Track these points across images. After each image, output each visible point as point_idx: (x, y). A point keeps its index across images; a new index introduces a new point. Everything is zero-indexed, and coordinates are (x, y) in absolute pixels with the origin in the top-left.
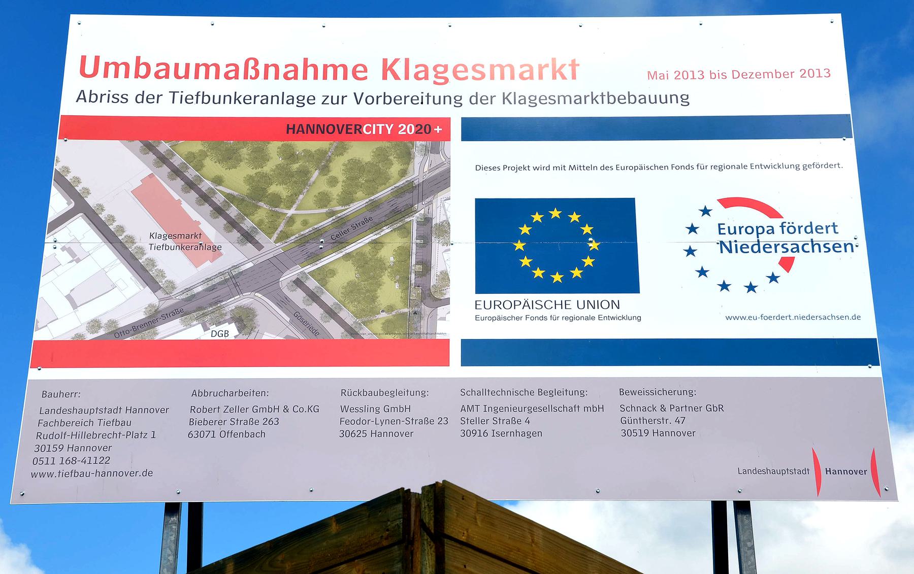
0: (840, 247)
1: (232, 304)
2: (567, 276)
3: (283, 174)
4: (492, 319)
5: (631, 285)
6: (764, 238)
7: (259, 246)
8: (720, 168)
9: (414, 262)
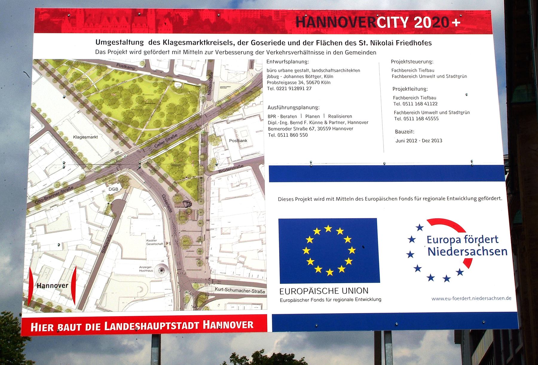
0: (499, 252)
1: (118, 174)
2: (336, 271)
3: (140, 111)
4: (291, 301)
5: (375, 277)
6: (455, 246)
7: (130, 147)
8: (429, 200)
9: (200, 154)
